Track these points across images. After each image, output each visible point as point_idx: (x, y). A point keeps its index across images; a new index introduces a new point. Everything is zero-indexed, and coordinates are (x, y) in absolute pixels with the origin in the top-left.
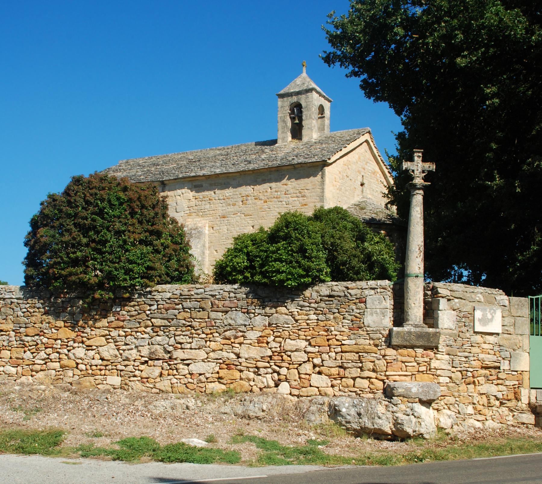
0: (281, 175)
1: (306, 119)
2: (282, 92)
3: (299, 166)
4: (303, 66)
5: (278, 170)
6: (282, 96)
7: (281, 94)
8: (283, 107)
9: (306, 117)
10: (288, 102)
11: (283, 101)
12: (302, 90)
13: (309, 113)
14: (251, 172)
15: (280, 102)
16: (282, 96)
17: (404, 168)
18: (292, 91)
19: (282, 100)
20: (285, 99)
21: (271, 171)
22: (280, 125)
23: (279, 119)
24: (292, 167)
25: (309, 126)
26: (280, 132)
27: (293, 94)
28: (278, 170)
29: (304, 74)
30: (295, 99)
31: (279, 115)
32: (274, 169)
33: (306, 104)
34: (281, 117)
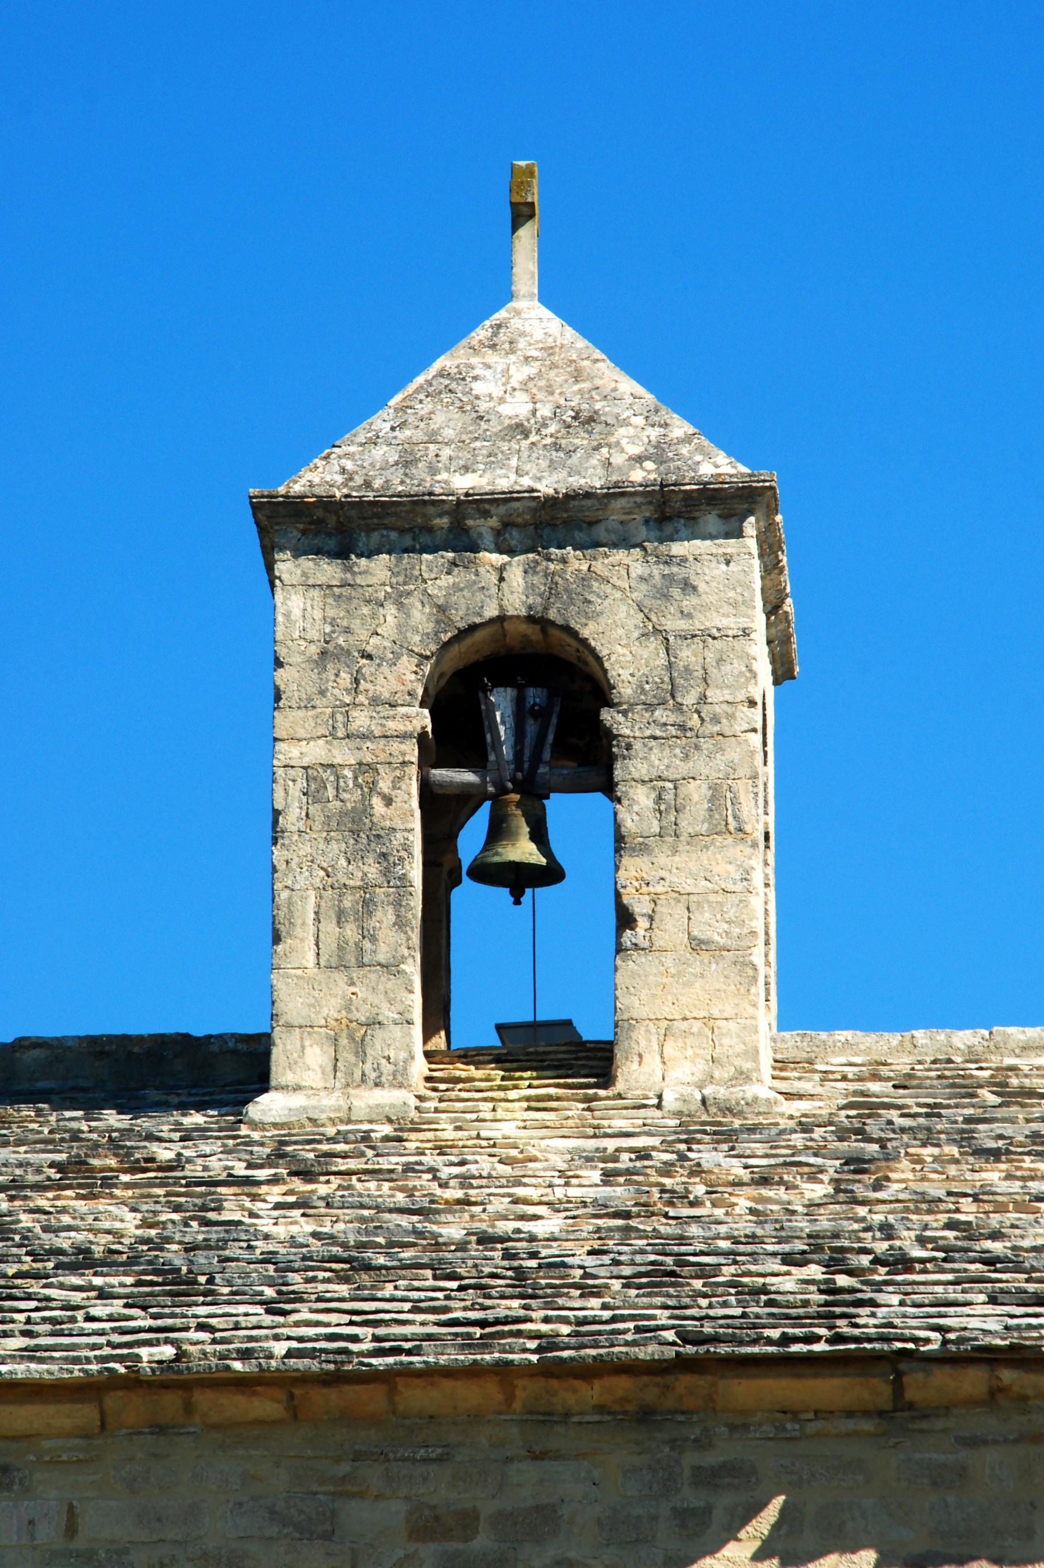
0: (706, 1478)
1: (669, 833)
2: (319, 477)
3: (973, 1381)
4: (521, 214)
5: (646, 1416)
6: (338, 529)
7: (327, 504)
8: (349, 669)
9: (668, 804)
10: (420, 616)
11: (339, 593)
12: (616, 493)
13: (707, 766)
14: (266, 1406)
15: (302, 597)
16: (338, 529)
17: (515, 1382)
18: (462, 483)
19: (328, 570)
20: (377, 570)
21: (546, 1417)
22: (307, 866)
23: (290, 797)
24: (876, 1390)
25: (709, 925)
26: (300, 951)
27: (484, 527)
28: (646, 1416)
29: (532, 318)
30: (504, 586)
31: (288, 752)
32: (594, 1392)
33: (652, 655)
34: (316, 780)
